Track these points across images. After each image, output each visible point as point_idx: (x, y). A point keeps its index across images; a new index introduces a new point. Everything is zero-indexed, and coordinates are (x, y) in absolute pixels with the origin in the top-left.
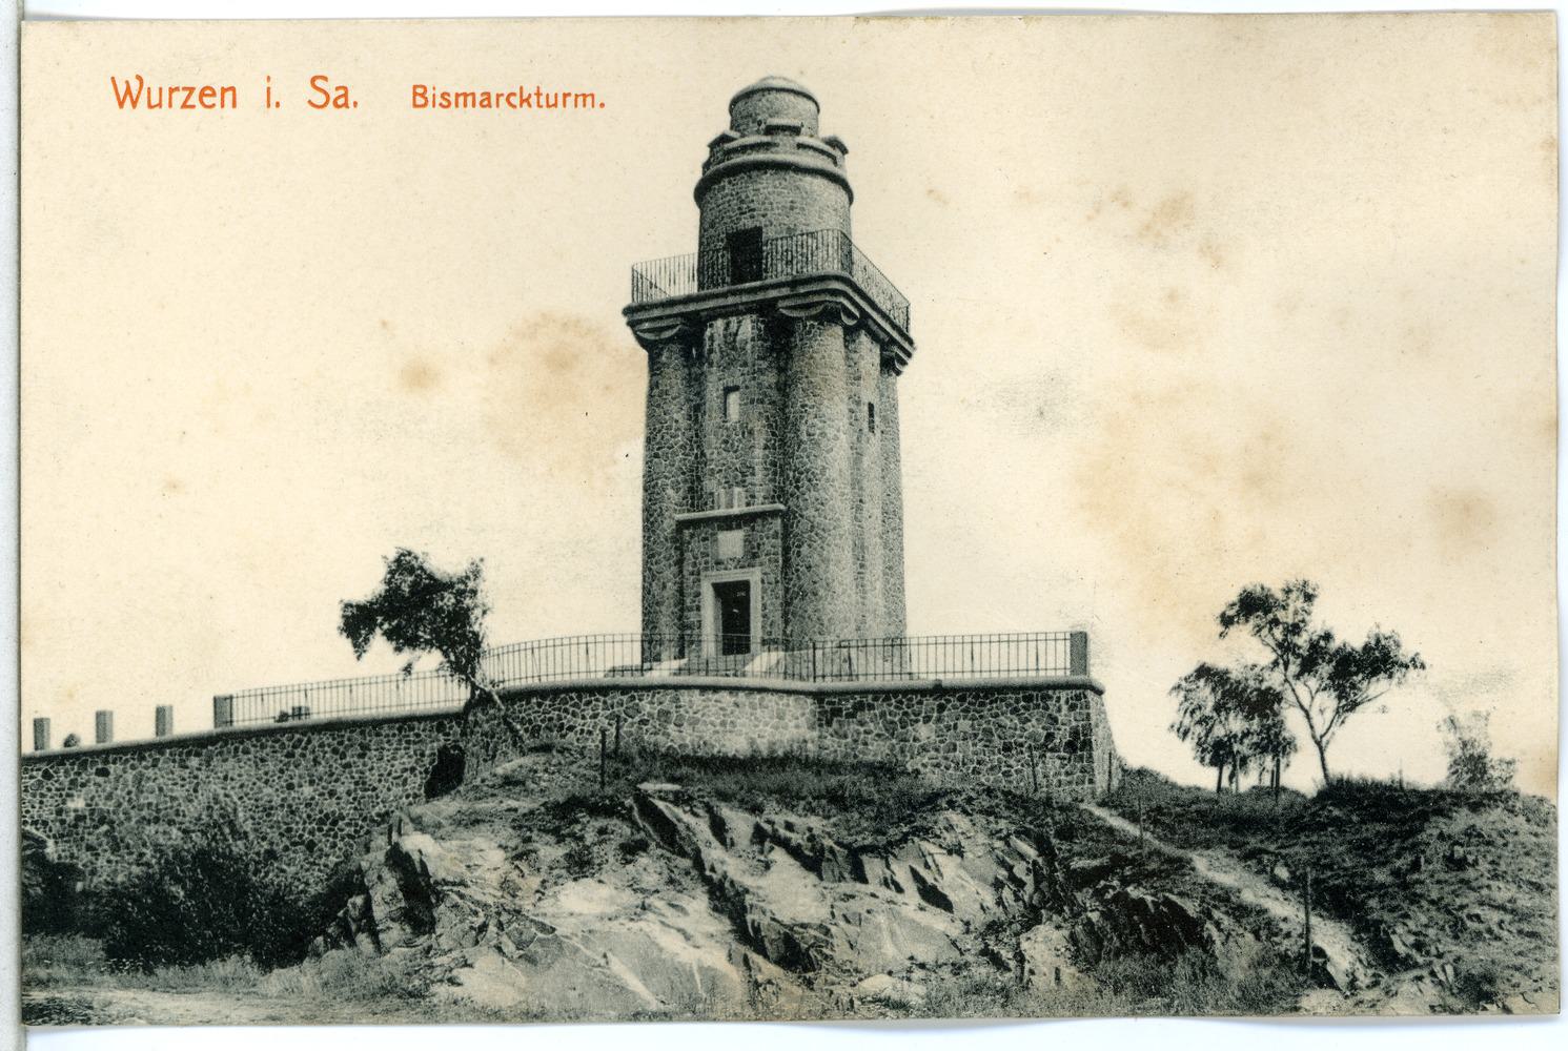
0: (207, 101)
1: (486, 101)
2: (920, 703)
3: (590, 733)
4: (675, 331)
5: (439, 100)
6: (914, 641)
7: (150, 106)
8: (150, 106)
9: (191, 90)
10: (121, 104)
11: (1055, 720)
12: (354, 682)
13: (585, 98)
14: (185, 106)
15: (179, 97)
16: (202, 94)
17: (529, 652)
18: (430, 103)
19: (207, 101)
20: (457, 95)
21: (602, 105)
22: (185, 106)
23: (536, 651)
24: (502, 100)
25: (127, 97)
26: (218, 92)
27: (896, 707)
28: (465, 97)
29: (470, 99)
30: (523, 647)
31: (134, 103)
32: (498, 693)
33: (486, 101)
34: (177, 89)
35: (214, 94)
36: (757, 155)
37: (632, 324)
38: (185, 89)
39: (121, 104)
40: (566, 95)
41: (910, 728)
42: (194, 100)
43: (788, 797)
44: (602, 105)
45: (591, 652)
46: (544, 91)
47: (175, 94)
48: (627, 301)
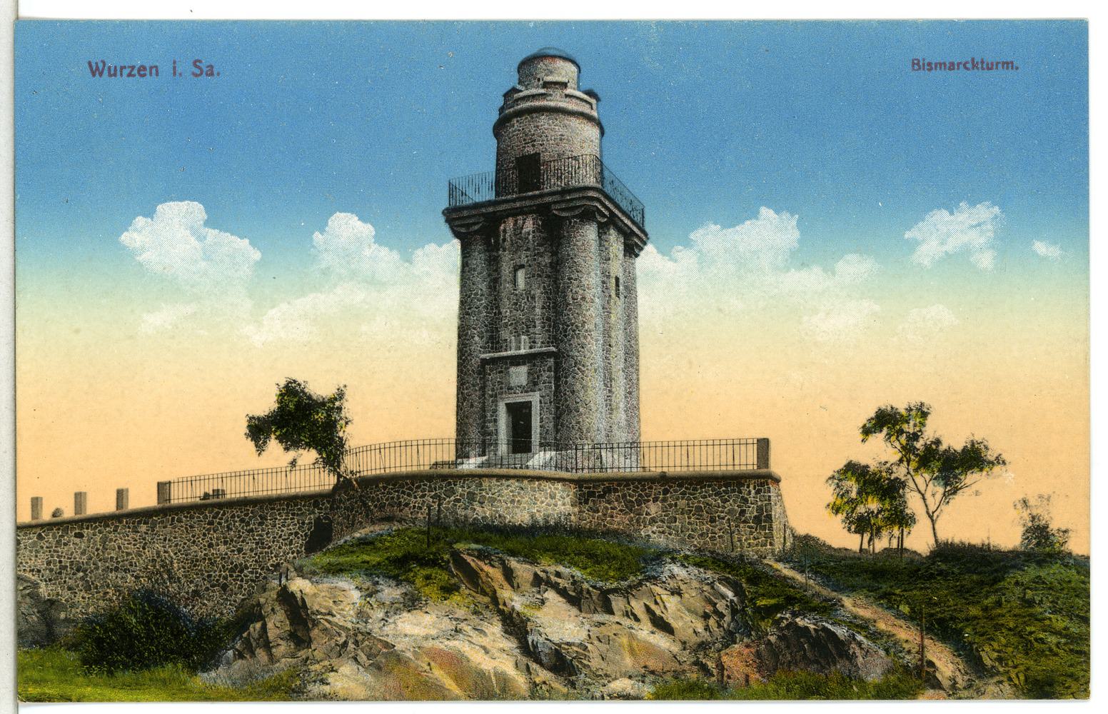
0: (142, 73)
1: (952, 66)
11: (746, 500)
13: (1008, 65)
14: (130, 75)
15: (126, 72)
16: (139, 70)
19: (142, 73)
21: (180, 74)
22: (130, 75)
28: (941, 65)
31: (101, 74)
38: (129, 67)
39: (94, 75)
41: (643, 505)
42: (135, 72)
44: (1017, 68)
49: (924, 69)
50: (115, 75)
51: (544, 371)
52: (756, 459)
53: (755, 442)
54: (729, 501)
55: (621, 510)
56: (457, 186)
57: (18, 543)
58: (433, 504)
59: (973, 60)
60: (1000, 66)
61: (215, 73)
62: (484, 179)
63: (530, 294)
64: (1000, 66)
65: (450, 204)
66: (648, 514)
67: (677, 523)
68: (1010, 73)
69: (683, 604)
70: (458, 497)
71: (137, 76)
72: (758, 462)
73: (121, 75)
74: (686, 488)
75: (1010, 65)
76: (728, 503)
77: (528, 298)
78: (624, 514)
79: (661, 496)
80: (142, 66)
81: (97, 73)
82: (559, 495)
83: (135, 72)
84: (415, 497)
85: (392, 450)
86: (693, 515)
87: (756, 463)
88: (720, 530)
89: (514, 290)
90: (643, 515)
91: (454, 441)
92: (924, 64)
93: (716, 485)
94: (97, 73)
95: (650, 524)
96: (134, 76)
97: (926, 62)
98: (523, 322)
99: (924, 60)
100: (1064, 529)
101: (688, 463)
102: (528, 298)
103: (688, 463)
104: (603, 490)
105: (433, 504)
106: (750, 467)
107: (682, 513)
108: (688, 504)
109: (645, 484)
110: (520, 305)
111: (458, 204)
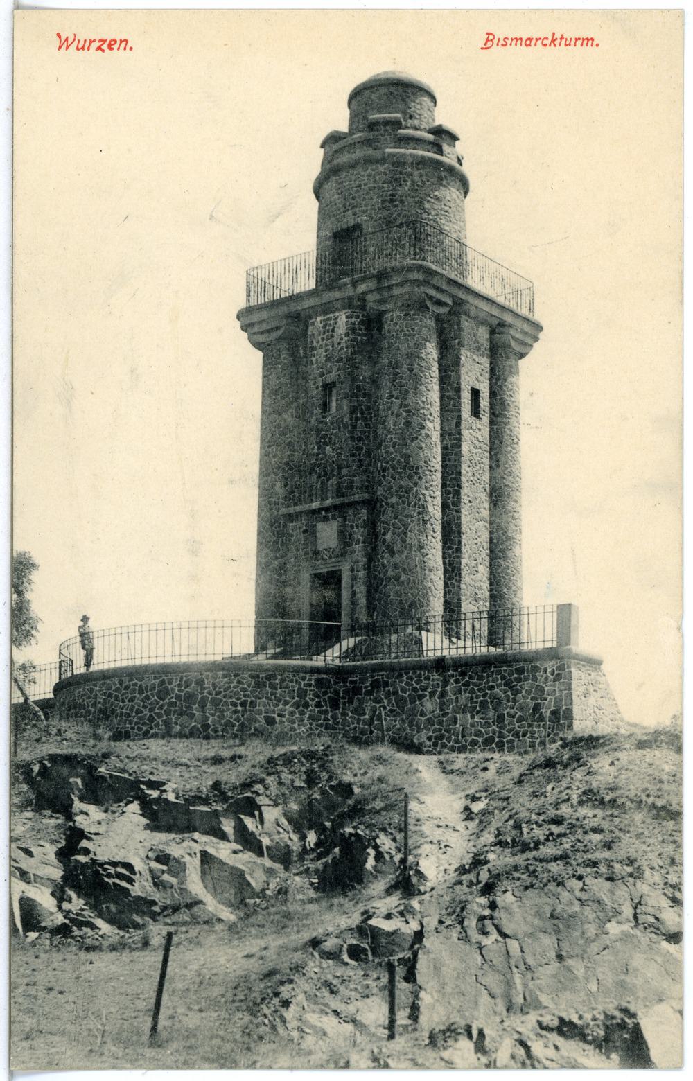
1: (529, 42)
3: (128, 715)
4: (280, 332)
6: (532, 610)
7: (78, 49)
8: (78, 49)
10: (60, 48)
11: (542, 691)
12: (131, 629)
17: (125, 636)
20: (512, 39)
25: (64, 43)
26: (118, 42)
27: (407, 684)
29: (519, 42)
30: (118, 631)
31: (67, 47)
33: (529, 42)
36: (388, 162)
37: (245, 328)
40: (576, 40)
41: (417, 703)
45: (177, 638)
46: (565, 37)
47: (93, 44)
48: (242, 304)
51: (357, 527)
52: (555, 635)
53: (555, 609)
54: (521, 692)
55: (392, 711)
56: (267, 281)
58: (143, 710)
62: (287, 268)
63: (342, 421)
65: (248, 301)
66: (423, 714)
67: (458, 726)
68: (589, 50)
69: (392, 837)
70: (174, 700)
72: (558, 637)
75: (590, 42)
76: (520, 695)
77: (339, 428)
78: (394, 716)
79: (440, 690)
82: (529, 700)
84: (123, 702)
86: (477, 713)
87: (555, 639)
88: (509, 731)
89: (323, 417)
90: (416, 716)
95: (425, 728)
98: (333, 462)
101: (206, 632)
102: (339, 428)
103: (206, 632)
104: (371, 684)
105: (143, 710)
106: (548, 645)
107: (464, 712)
108: (472, 698)
109: (420, 674)
110: (330, 438)
111: (266, 300)
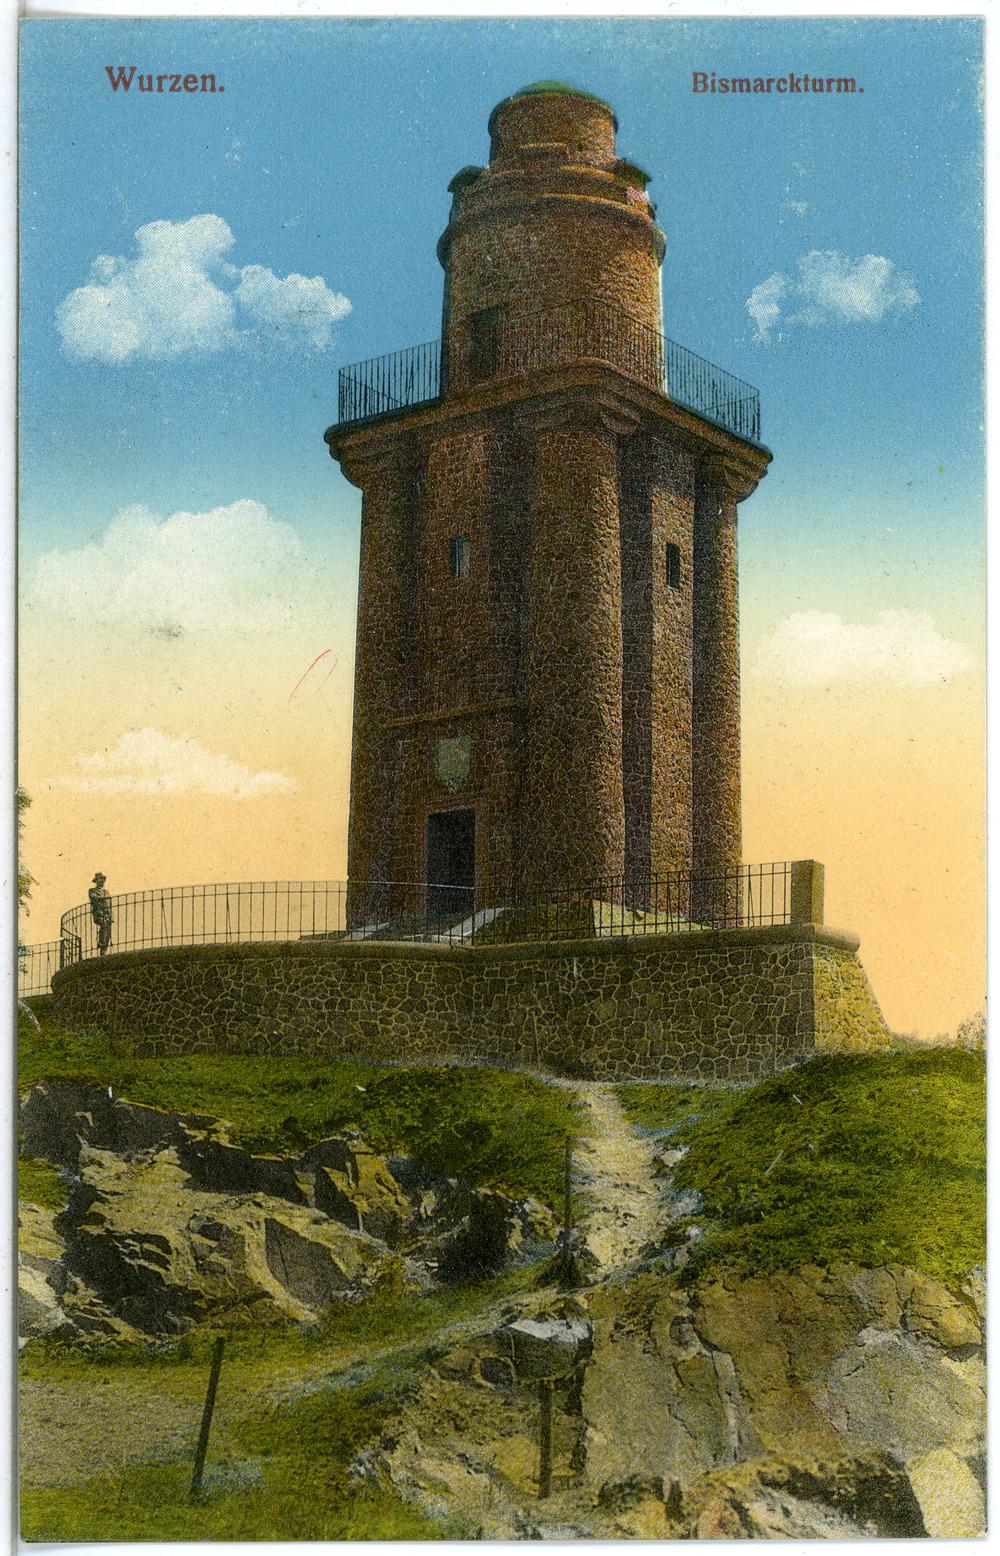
0: (191, 86)
2: (601, 968)
5: (730, 85)
9: (178, 77)
13: (846, 84)
14: (172, 89)
15: (167, 84)
16: (186, 82)
17: (158, 904)
18: (710, 88)
19: (191, 86)
21: (222, 89)
22: (172, 89)
23: (167, 903)
24: (774, 85)
28: (819, 86)
31: (127, 85)
32: (358, 1228)
34: (165, 76)
35: (195, 81)
38: (172, 77)
39: (115, 85)
42: (181, 83)
43: (149, 1242)
44: (862, 90)
46: (811, 78)
49: (713, 90)
50: (821, 90)
53: (789, 869)
57: (17, 1224)
59: (792, 76)
60: (834, 86)
61: (217, 87)
64: (834, 86)
71: (183, 89)
73: (160, 89)
74: (664, 968)
80: (190, 76)
81: (121, 83)
83: (181, 83)
85: (188, 901)
87: (788, 911)
91: (345, 888)
92: (713, 82)
93: (715, 959)
94: (121, 83)
96: (179, 89)
97: (717, 78)
99: (133, 69)
100: (861, 963)
106: (779, 921)
